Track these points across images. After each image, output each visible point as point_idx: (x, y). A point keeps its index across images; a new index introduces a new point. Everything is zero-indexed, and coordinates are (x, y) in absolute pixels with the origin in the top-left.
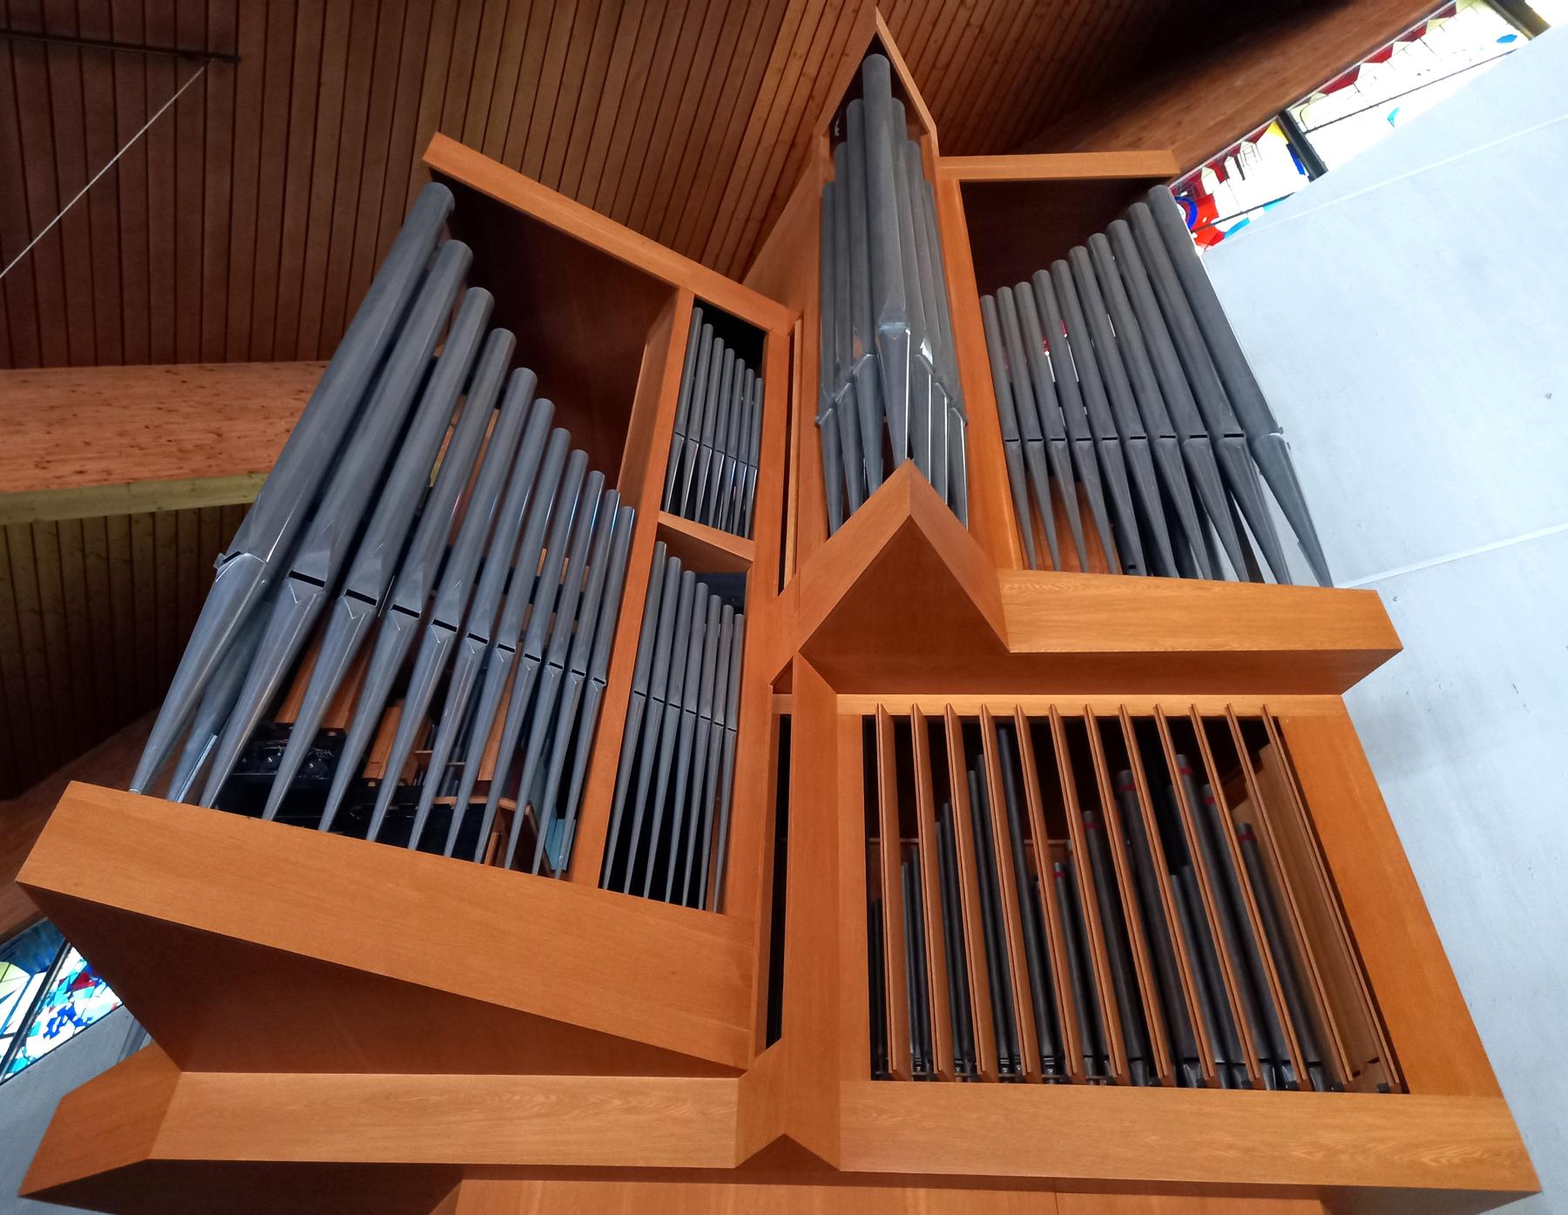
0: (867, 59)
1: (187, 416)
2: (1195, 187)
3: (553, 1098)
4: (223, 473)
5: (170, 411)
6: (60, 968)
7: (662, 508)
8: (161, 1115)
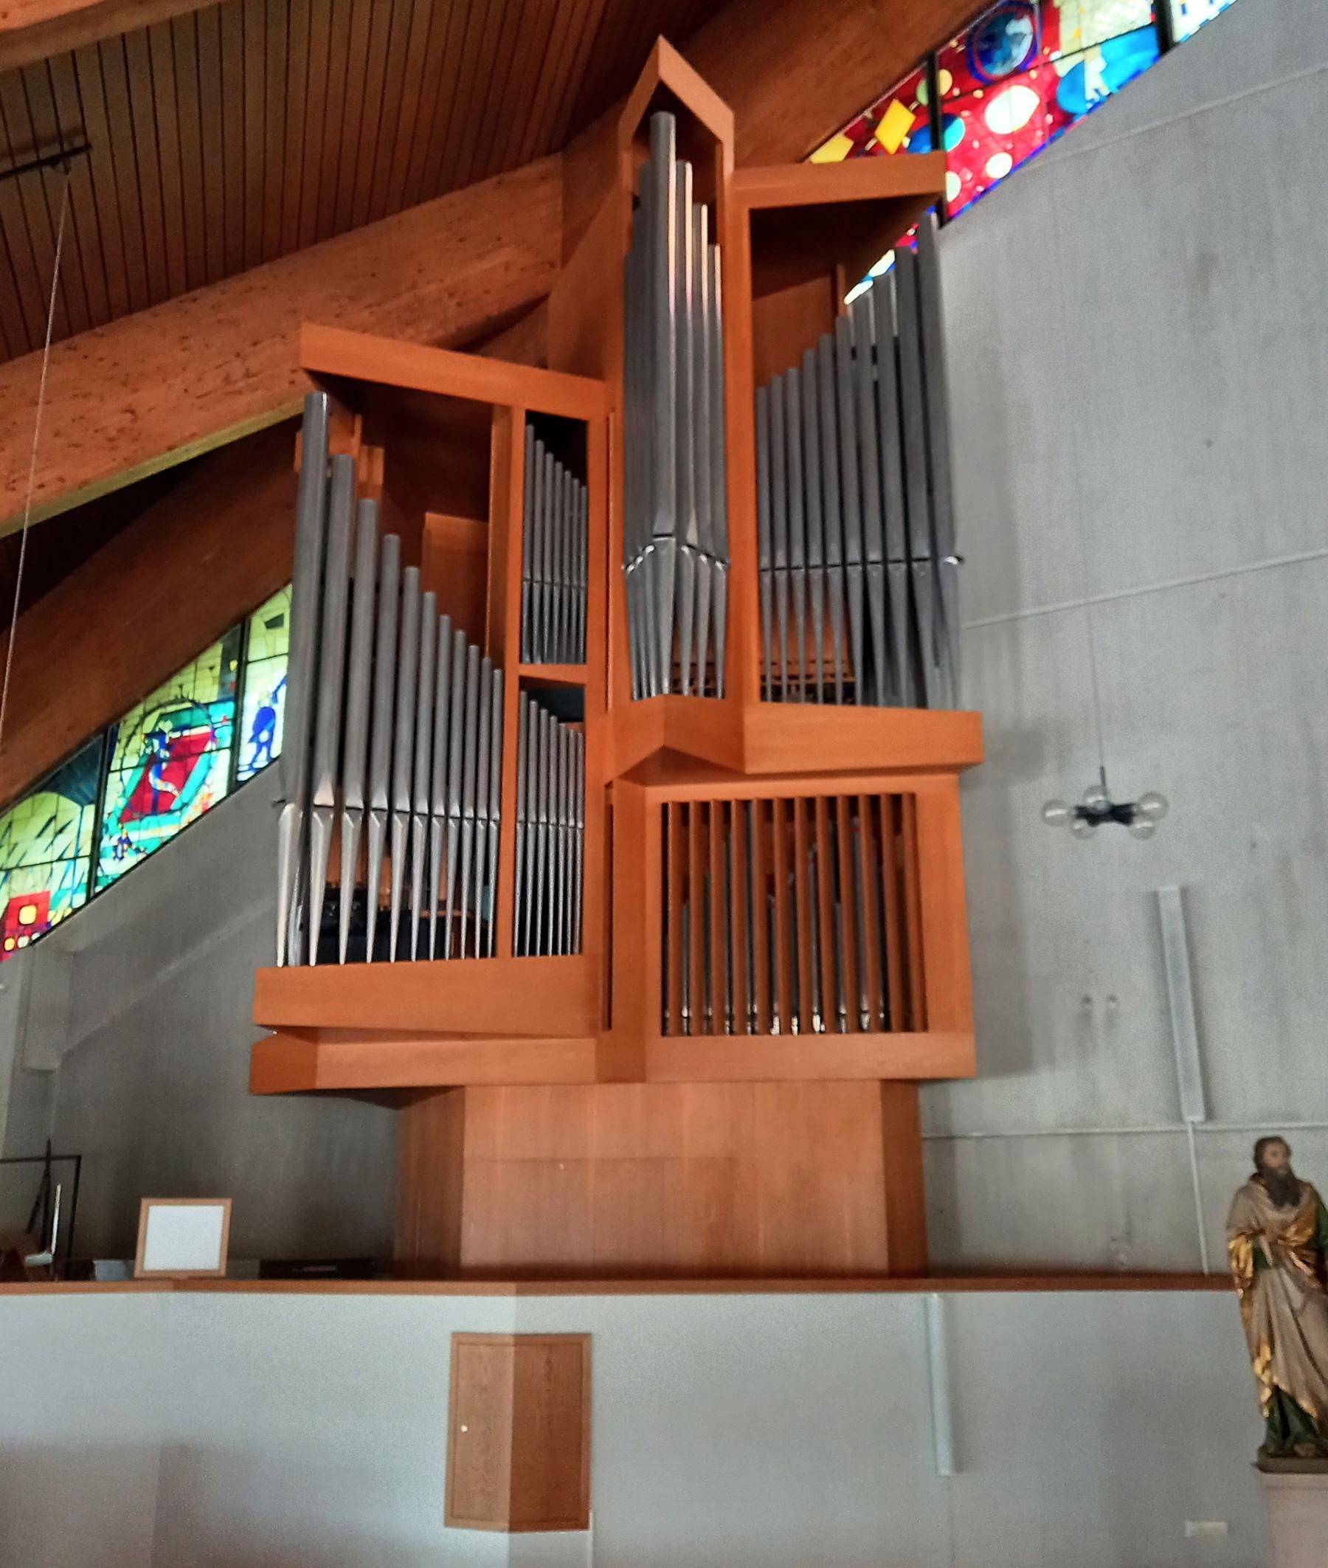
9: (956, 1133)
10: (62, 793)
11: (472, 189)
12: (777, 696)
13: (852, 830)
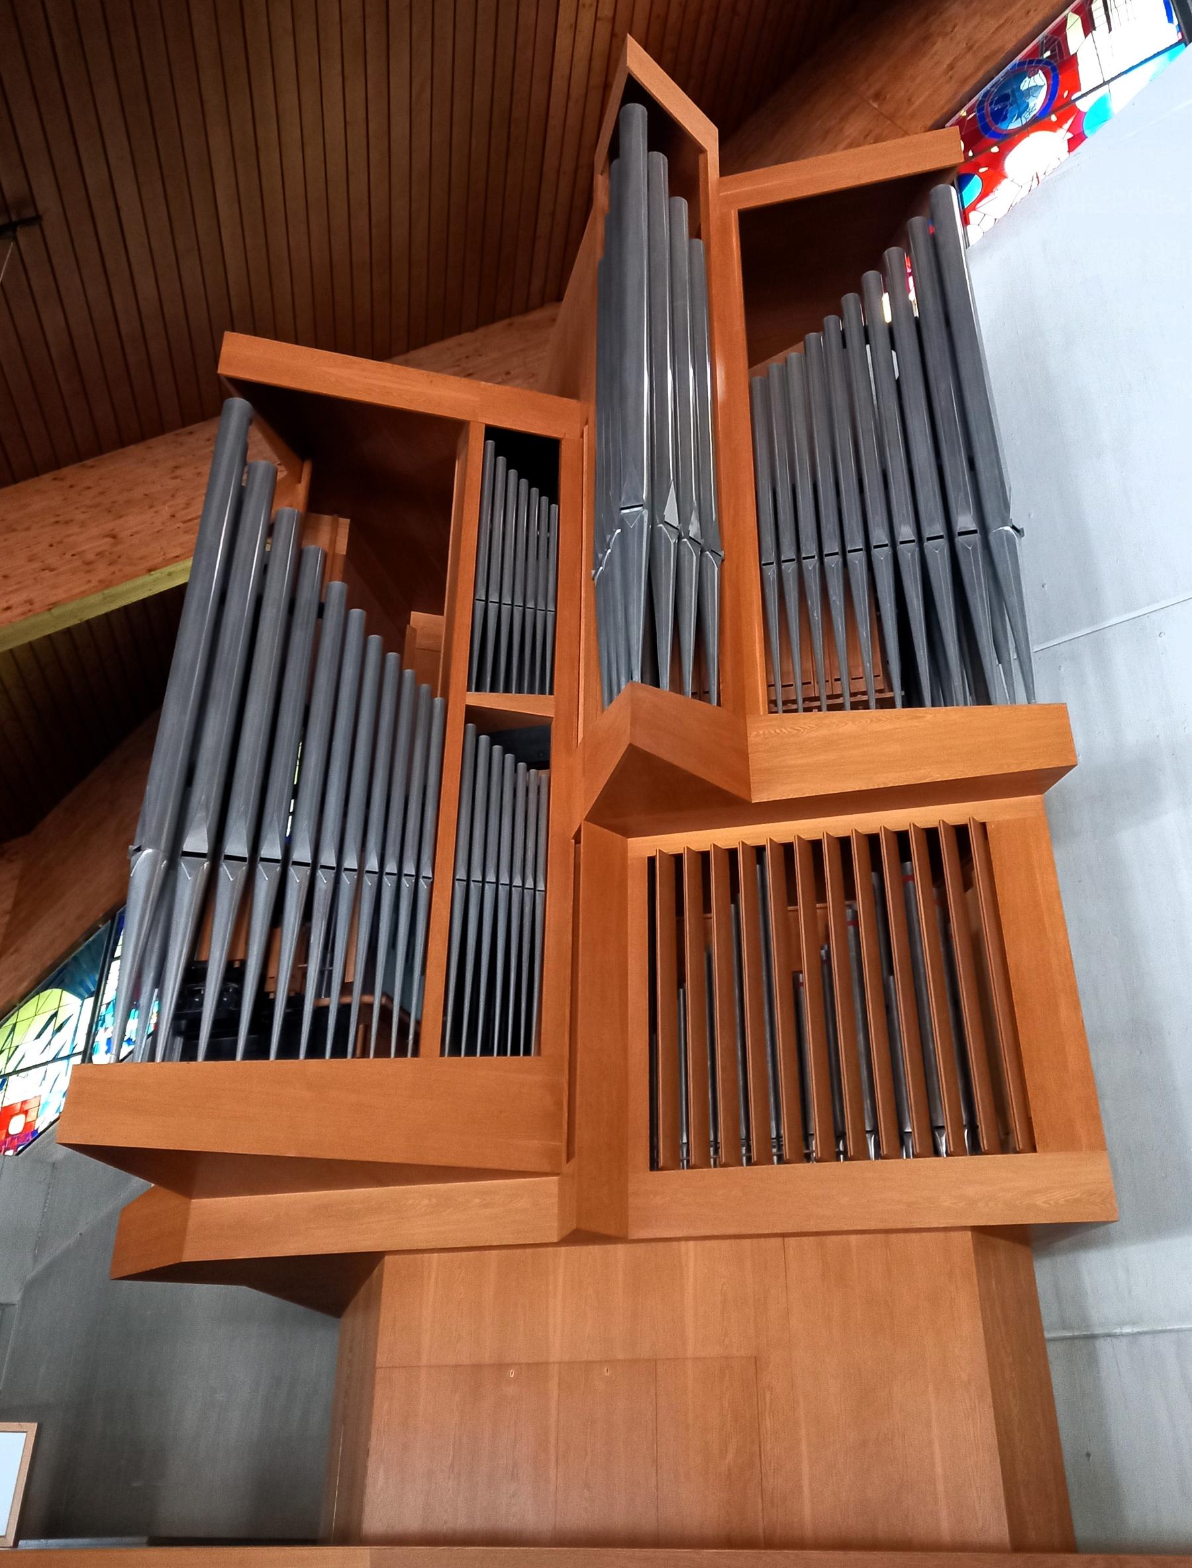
0: (623, 108)
1: (83, 524)
2: (1059, 44)
3: (434, 1201)
4: (128, 578)
5: (66, 523)
6: (103, 993)
7: (469, 689)
8: (183, 1231)
9: (1098, 1331)
10: (64, 988)
11: (481, 331)
12: (789, 706)
13: (905, 880)
